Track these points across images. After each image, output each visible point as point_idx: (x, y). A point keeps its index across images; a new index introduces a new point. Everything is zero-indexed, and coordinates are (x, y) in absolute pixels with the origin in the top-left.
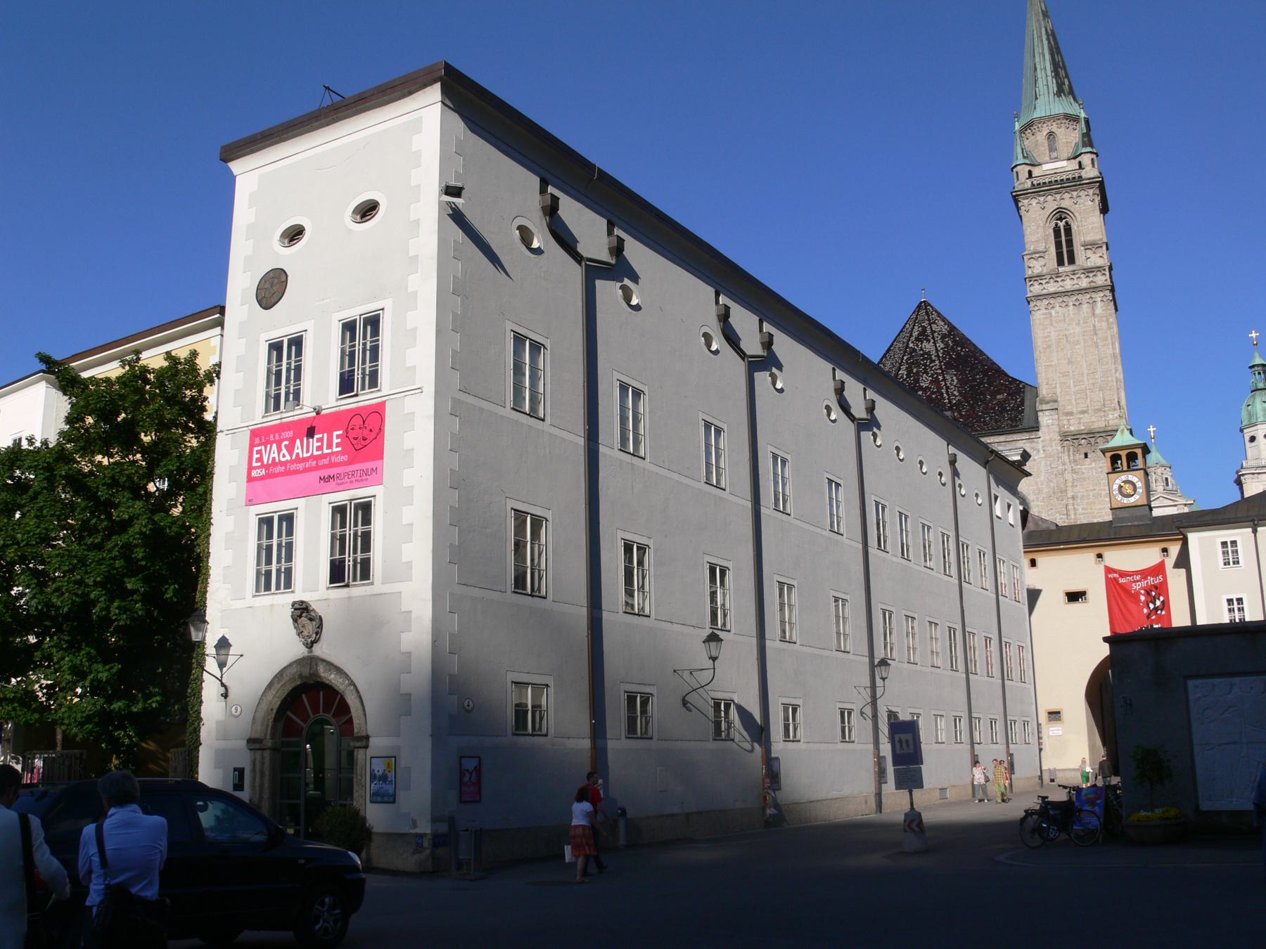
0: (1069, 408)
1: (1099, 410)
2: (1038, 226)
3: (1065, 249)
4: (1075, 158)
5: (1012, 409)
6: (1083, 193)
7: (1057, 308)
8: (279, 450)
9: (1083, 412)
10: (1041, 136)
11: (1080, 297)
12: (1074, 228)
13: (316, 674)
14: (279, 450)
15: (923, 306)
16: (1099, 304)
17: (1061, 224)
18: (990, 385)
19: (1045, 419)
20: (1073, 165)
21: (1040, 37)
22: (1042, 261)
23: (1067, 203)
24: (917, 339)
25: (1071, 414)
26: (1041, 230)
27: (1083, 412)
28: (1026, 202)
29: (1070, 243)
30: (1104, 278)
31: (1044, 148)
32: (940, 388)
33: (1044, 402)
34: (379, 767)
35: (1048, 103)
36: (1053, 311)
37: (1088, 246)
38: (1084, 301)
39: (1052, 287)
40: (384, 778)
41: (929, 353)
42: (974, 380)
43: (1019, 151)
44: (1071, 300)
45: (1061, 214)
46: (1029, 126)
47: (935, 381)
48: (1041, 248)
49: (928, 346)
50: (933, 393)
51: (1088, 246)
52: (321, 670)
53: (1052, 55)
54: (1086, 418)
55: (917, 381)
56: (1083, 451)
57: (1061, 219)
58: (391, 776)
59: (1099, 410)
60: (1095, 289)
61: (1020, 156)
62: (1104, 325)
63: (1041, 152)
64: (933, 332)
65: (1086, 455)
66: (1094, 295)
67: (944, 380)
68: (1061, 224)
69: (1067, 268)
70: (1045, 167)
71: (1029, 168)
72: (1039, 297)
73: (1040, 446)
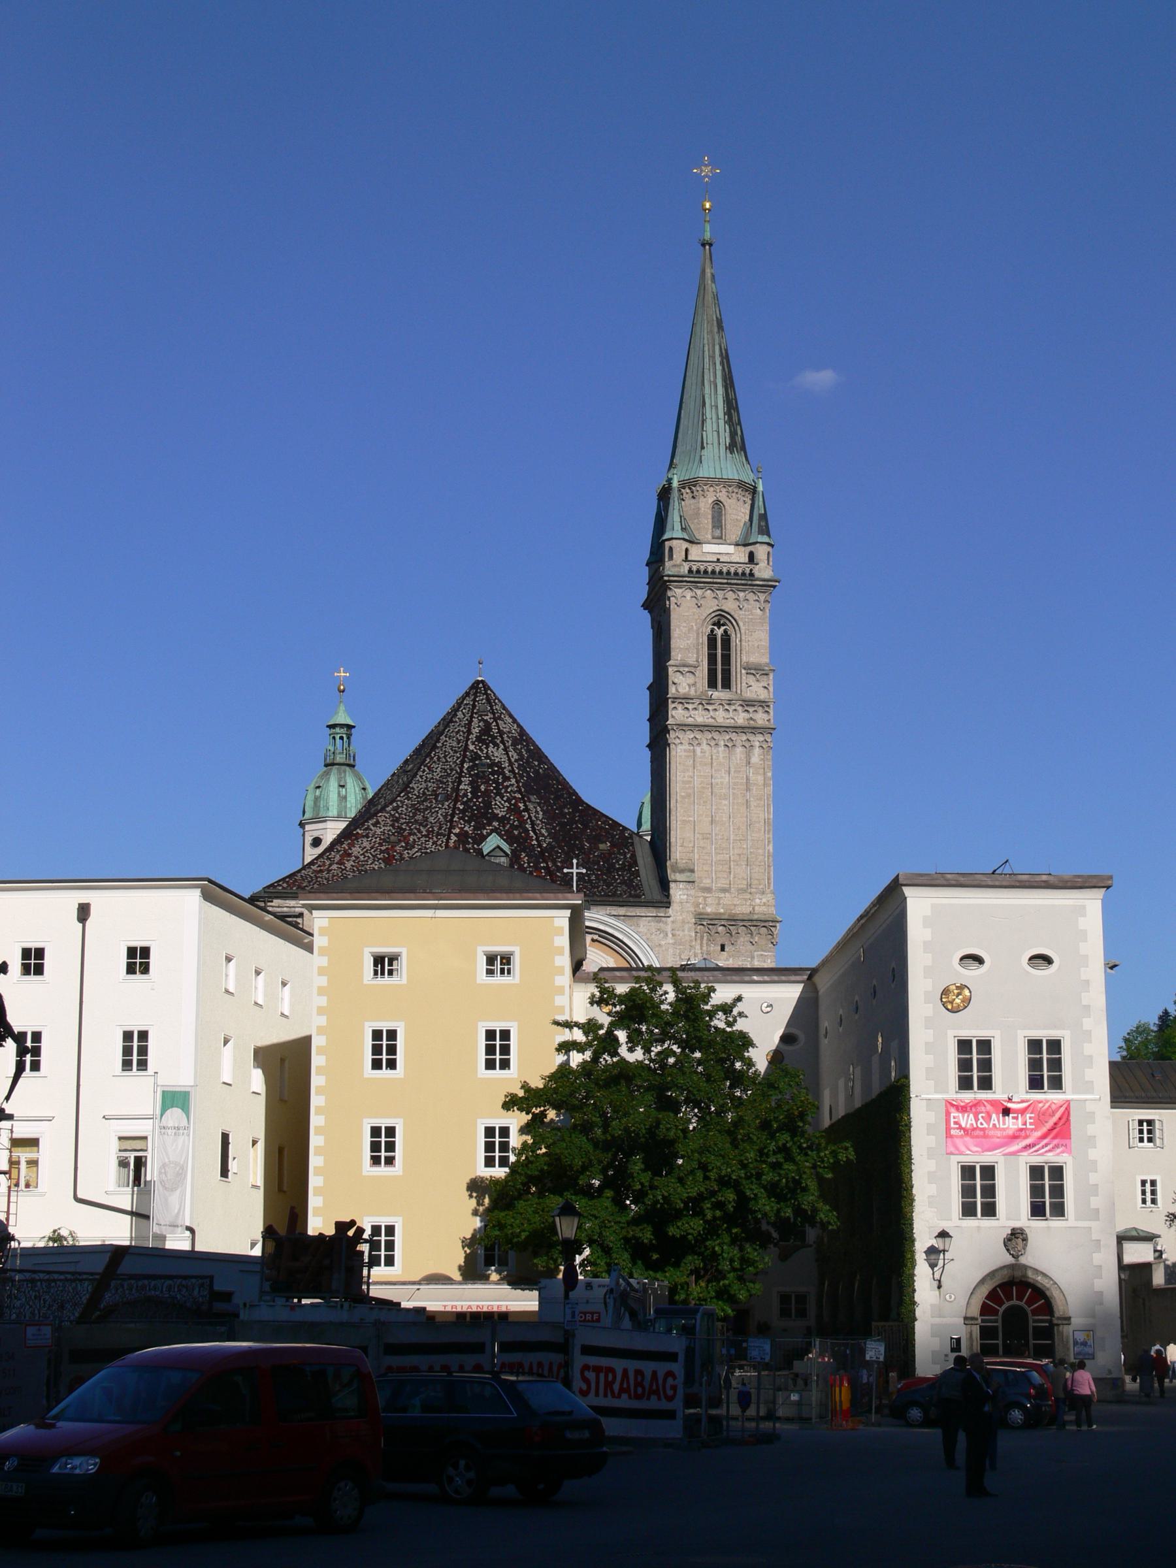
0: (707, 882)
1: (744, 891)
2: (690, 629)
3: (720, 672)
4: (745, 545)
5: (622, 868)
6: (751, 597)
7: (705, 746)
8: (977, 1119)
9: (724, 890)
10: (705, 505)
11: (734, 736)
12: (735, 641)
13: (1025, 1276)
14: (977, 1119)
15: (479, 688)
16: (757, 751)
17: (719, 632)
18: (586, 826)
19: (678, 892)
20: (741, 555)
21: (712, 357)
22: (690, 679)
23: (730, 606)
24: (479, 739)
25: (708, 890)
26: (693, 635)
27: (724, 890)
28: (678, 591)
29: (727, 659)
30: (765, 716)
31: (707, 522)
32: (522, 822)
33: (677, 870)
34: (1080, 1337)
35: (716, 462)
36: (698, 749)
37: (754, 670)
38: (739, 743)
39: (700, 717)
40: (1084, 1344)
41: (499, 764)
42: (563, 815)
43: (677, 519)
44: (723, 739)
45: (720, 618)
46: (690, 484)
47: (514, 810)
48: (691, 660)
49: (498, 754)
50: (513, 827)
51: (754, 670)
52: (1030, 1274)
53: (726, 387)
54: (727, 899)
55: (488, 805)
56: (720, 941)
57: (718, 624)
58: (1090, 1342)
59: (744, 891)
60: (754, 730)
61: (677, 526)
62: (760, 779)
63: (703, 526)
64: (501, 733)
65: (723, 948)
66: (752, 737)
67: (527, 810)
68: (719, 632)
69: (719, 694)
70: (707, 548)
71: (685, 545)
72: (683, 727)
73: (669, 928)
